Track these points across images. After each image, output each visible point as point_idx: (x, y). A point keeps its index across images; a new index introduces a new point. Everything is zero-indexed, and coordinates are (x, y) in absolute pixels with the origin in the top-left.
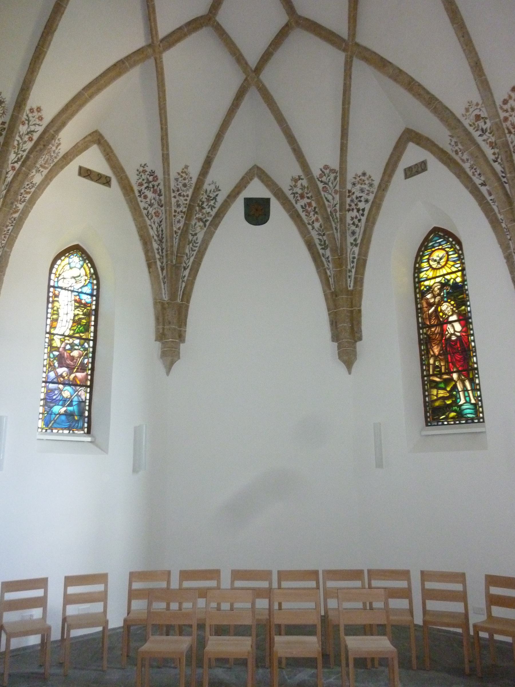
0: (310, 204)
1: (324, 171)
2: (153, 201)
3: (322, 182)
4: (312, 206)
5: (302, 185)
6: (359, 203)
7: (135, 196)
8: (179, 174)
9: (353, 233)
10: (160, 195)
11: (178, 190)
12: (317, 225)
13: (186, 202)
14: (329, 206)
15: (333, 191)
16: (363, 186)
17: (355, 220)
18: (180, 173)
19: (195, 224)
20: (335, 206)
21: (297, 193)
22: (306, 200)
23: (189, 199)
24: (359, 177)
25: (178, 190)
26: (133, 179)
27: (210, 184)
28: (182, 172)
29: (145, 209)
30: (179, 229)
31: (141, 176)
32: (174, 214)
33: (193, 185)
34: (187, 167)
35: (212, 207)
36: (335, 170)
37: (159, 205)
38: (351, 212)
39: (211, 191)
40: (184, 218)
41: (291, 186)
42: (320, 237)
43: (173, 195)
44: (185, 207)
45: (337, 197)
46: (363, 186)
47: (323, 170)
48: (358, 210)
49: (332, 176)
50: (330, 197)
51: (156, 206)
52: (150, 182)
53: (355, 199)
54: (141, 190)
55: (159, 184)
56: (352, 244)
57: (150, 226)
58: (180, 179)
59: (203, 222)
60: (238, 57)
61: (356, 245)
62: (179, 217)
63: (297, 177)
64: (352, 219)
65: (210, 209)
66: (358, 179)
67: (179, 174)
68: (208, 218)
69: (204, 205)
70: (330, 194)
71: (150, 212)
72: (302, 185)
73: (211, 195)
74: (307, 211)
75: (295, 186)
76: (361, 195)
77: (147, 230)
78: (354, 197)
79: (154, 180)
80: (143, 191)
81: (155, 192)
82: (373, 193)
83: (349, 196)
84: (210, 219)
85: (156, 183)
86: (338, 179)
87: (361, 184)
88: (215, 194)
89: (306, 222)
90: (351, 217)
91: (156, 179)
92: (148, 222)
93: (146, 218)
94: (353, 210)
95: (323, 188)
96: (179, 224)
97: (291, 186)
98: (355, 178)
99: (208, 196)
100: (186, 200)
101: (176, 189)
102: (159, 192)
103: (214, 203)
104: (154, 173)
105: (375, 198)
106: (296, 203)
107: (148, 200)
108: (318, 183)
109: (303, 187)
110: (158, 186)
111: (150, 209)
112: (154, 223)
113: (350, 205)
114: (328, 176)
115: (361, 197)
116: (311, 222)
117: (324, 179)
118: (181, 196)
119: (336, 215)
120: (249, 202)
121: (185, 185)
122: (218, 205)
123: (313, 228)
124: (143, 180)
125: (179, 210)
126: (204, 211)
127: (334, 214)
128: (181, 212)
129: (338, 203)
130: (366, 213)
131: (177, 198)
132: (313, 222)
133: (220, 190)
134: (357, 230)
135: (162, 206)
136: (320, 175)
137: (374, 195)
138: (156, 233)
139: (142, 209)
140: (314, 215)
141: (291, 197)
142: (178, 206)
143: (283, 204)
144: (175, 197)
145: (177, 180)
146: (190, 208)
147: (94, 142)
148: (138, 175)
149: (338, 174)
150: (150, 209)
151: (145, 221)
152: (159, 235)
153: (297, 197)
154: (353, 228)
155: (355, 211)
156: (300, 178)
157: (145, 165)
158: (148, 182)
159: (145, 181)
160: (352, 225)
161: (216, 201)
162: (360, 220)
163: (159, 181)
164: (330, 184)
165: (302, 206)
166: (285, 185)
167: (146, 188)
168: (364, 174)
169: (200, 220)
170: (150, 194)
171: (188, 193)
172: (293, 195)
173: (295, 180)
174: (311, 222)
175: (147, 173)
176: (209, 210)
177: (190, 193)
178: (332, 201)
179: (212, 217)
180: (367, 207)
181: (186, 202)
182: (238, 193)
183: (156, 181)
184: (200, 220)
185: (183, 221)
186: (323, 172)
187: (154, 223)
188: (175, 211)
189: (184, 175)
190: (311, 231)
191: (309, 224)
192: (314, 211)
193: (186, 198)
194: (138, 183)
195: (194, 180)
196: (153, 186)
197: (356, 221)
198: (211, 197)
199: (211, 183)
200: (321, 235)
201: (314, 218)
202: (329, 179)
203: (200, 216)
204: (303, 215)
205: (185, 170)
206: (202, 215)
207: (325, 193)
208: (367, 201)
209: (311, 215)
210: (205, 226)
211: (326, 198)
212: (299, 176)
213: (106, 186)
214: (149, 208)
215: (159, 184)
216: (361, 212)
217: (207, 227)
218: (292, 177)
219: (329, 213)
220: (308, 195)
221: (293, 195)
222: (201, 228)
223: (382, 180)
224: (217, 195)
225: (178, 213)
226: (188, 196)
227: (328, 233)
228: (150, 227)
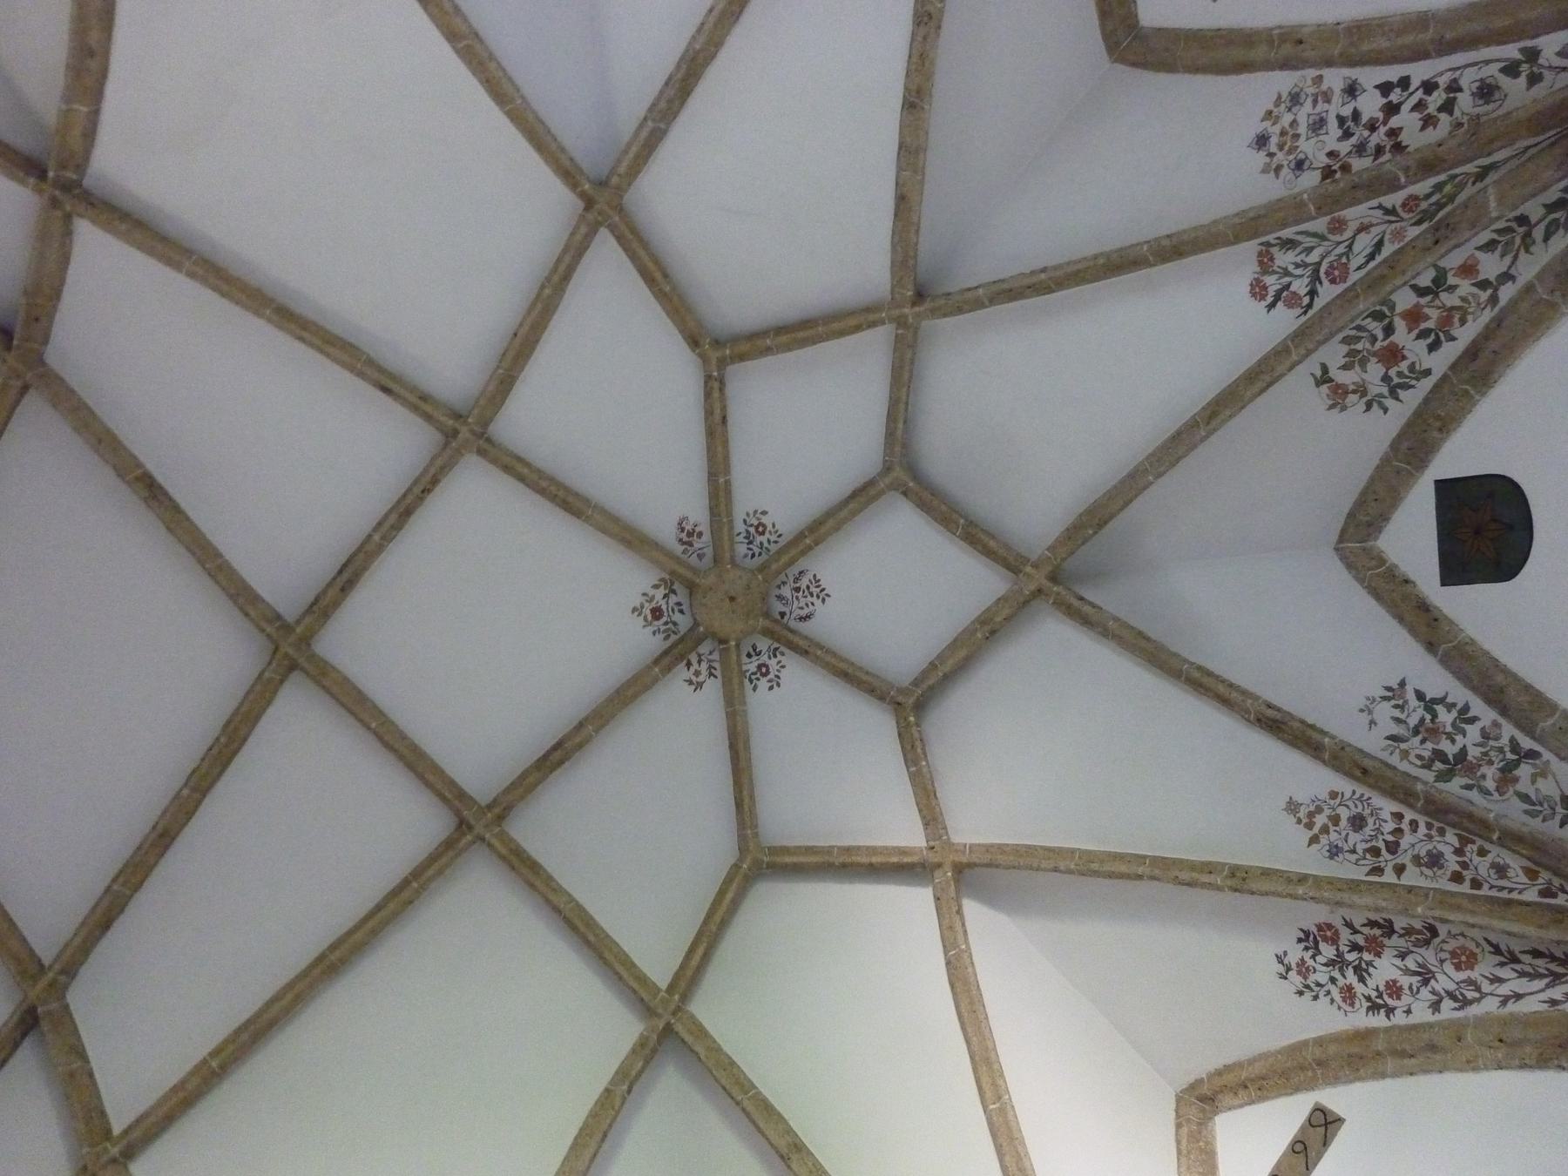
0: (1414, 317)
1: (1272, 291)
2: (1410, 963)
3: (1313, 293)
4: (1417, 305)
5: (1345, 367)
6: (1365, 119)
7: (1387, 1030)
8: (1314, 840)
9: (1486, 91)
10: (1389, 929)
11: (1375, 852)
12: (1490, 266)
13: (1422, 829)
14: (1398, 235)
15: (1338, 238)
16: (1302, 129)
17: (1432, 109)
18: (1310, 834)
19: (1525, 798)
20: (1391, 212)
21: (1386, 379)
22: (1402, 336)
23: (1409, 815)
24: (1271, 155)
25: (1375, 852)
26: (1324, 1019)
27: (1372, 723)
28: (1310, 826)
29: (1436, 1006)
30: (1532, 874)
31: (1318, 985)
32: (1465, 888)
33: (1361, 790)
34: (1292, 807)
35: (1465, 716)
36: (1260, 254)
37: (1427, 943)
38: (1404, 138)
39: (1398, 720)
40: (1487, 846)
41: (1369, 406)
42: (1538, 234)
43: (1389, 877)
44: (1442, 832)
45: (1354, 214)
46: (1302, 129)
47: (1270, 299)
48: (1392, 109)
49: (1284, 259)
50: (1364, 243)
51: (1429, 955)
52: (1340, 955)
53: (1353, 140)
54: (1368, 998)
55: (1349, 925)
56: (1534, 79)
57: (1504, 1002)
58: (1333, 836)
59: (1517, 764)
60: (985, 634)
61: (1532, 55)
62: (1482, 866)
63: (1325, 388)
64: (1429, 121)
65: (1467, 727)
66: (1280, 156)
67: (1314, 840)
68: (1505, 741)
69: (1450, 749)
70: (1350, 247)
71: (1452, 987)
72: (1345, 367)
73: (1413, 721)
74: (1446, 321)
75: (1361, 390)
76: (1333, 124)
77: (1514, 1019)
78: (1344, 147)
79: (1334, 940)
80: (1374, 994)
81: (1376, 948)
82: (1320, 77)
83: (1346, 168)
84: (1508, 730)
85: (1345, 935)
86: (1287, 233)
87: (1297, 136)
88: (1413, 702)
89: (1487, 316)
90: (1423, 128)
91: (1327, 932)
92: (1490, 1006)
93: (1474, 1010)
94: (1393, 133)
95: (1333, 281)
96: (1511, 873)
97: (1369, 406)
98: (1278, 169)
99: (1416, 732)
100: (1414, 825)
101: (1370, 860)
102: (1377, 932)
103: (1450, 707)
104: (1307, 934)
105: (1329, 63)
106: (1428, 372)
107: (1405, 981)
108: (1319, 303)
109: (1354, 360)
110: (1356, 932)
111: (1442, 983)
112: (1500, 980)
113: (1379, 150)
114: (1286, 273)
115: (1341, 120)
116: (1484, 296)
117: (1300, 286)
118: (1397, 844)
119: (1428, 196)
120: (1460, 564)
121: (1358, 822)
122: (1460, 694)
123: (1507, 277)
124: (1333, 980)
125: (1452, 863)
126: (1474, 753)
127: (1424, 205)
128: (1459, 852)
129: (1374, 203)
130: (1392, 73)
131: (1406, 859)
132: (1483, 285)
133: (1402, 684)
134: (1468, 80)
135: (1434, 932)
136: (1289, 305)
137: (1326, 72)
138: (1539, 984)
139: (1437, 1017)
140: (1452, 288)
141: (1412, 399)
142: (1435, 860)
143: (1447, 425)
144: (1400, 870)
145: (1334, 851)
146: (1440, 812)
147: (1205, 1121)
148: (1316, 998)
149: (1270, 238)
150: (1442, 983)
151: (1480, 1022)
152: (1551, 973)
153: (1400, 374)
154: (1465, 101)
155: (1395, 122)
156: (1324, 378)
157: (1280, 960)
158: (1338, 962)
159: (1336, 974)
160: (1457, 113)
161: (1441, 701)
162: (1429, 87)
163: (1338, 923)
164: (1314, 257)
165: (1433, 347)
166: (1371, 433)
167: (1362, 980)
168: (1261, 141)
169: (1507, 776)
170: (1385, 969)
171: (1386, 815)
172: (1402, 394)
173: (1339, 397)
174: (1484, 296)
175: (1310, 962)
176: (1473, 732)
177: (1387, 807)
178: (1375, 231)
179: (1501, 720)
180: (1370, 77)
181: (1422, 829)
182: (1424, 607)
183: (1337, 933)
184: (1507, 776)
185: (1497, 854)
186: (1277, 297)
187: (1500, 980)
188: (1457, 878)
189: (1320, 820)
190: (1522, 281)
191: (1494, 300)
192: (1436, 295)
193: (1405, 826)
194: (1343, 1005)
195: (1345, 786)
196: (1355, 947)
197: (1437, 98)
198: (1422, 720)
199: (1364, 719)
200: (1528, 235)
201: (1465, 287)
202: (1297, 266)
203: (1490, 773)
204: (1465, 335)
205: (1304, 815)
206: (1491, 763)
207: (1354, 264)
208: (1352, 90)
209: (1458, 303)
210: (1532, 755)
211: (1371, 257)
212: (1319, 383)
213: (1334, 1135)
214: (1438, 988)
215: (1349, 925)
216: (1395, 96)
217: (1537, 747)
218: (1331, 407)
219: (1425, 225)
220: (1380, 336)
221: (1402, 394)
222: (1544, 773)
223: (1268, 66)
224: (1420, 696)
225: (1464, 865)
226: (1399, 817)
227: (1493, 204)
228: (1512, 1007)
